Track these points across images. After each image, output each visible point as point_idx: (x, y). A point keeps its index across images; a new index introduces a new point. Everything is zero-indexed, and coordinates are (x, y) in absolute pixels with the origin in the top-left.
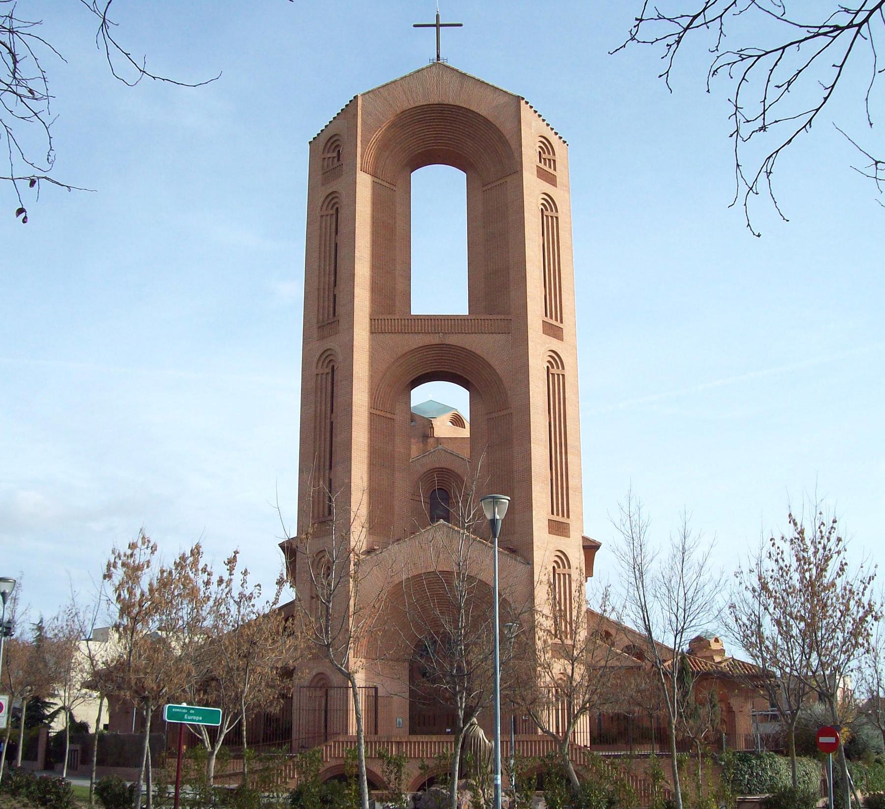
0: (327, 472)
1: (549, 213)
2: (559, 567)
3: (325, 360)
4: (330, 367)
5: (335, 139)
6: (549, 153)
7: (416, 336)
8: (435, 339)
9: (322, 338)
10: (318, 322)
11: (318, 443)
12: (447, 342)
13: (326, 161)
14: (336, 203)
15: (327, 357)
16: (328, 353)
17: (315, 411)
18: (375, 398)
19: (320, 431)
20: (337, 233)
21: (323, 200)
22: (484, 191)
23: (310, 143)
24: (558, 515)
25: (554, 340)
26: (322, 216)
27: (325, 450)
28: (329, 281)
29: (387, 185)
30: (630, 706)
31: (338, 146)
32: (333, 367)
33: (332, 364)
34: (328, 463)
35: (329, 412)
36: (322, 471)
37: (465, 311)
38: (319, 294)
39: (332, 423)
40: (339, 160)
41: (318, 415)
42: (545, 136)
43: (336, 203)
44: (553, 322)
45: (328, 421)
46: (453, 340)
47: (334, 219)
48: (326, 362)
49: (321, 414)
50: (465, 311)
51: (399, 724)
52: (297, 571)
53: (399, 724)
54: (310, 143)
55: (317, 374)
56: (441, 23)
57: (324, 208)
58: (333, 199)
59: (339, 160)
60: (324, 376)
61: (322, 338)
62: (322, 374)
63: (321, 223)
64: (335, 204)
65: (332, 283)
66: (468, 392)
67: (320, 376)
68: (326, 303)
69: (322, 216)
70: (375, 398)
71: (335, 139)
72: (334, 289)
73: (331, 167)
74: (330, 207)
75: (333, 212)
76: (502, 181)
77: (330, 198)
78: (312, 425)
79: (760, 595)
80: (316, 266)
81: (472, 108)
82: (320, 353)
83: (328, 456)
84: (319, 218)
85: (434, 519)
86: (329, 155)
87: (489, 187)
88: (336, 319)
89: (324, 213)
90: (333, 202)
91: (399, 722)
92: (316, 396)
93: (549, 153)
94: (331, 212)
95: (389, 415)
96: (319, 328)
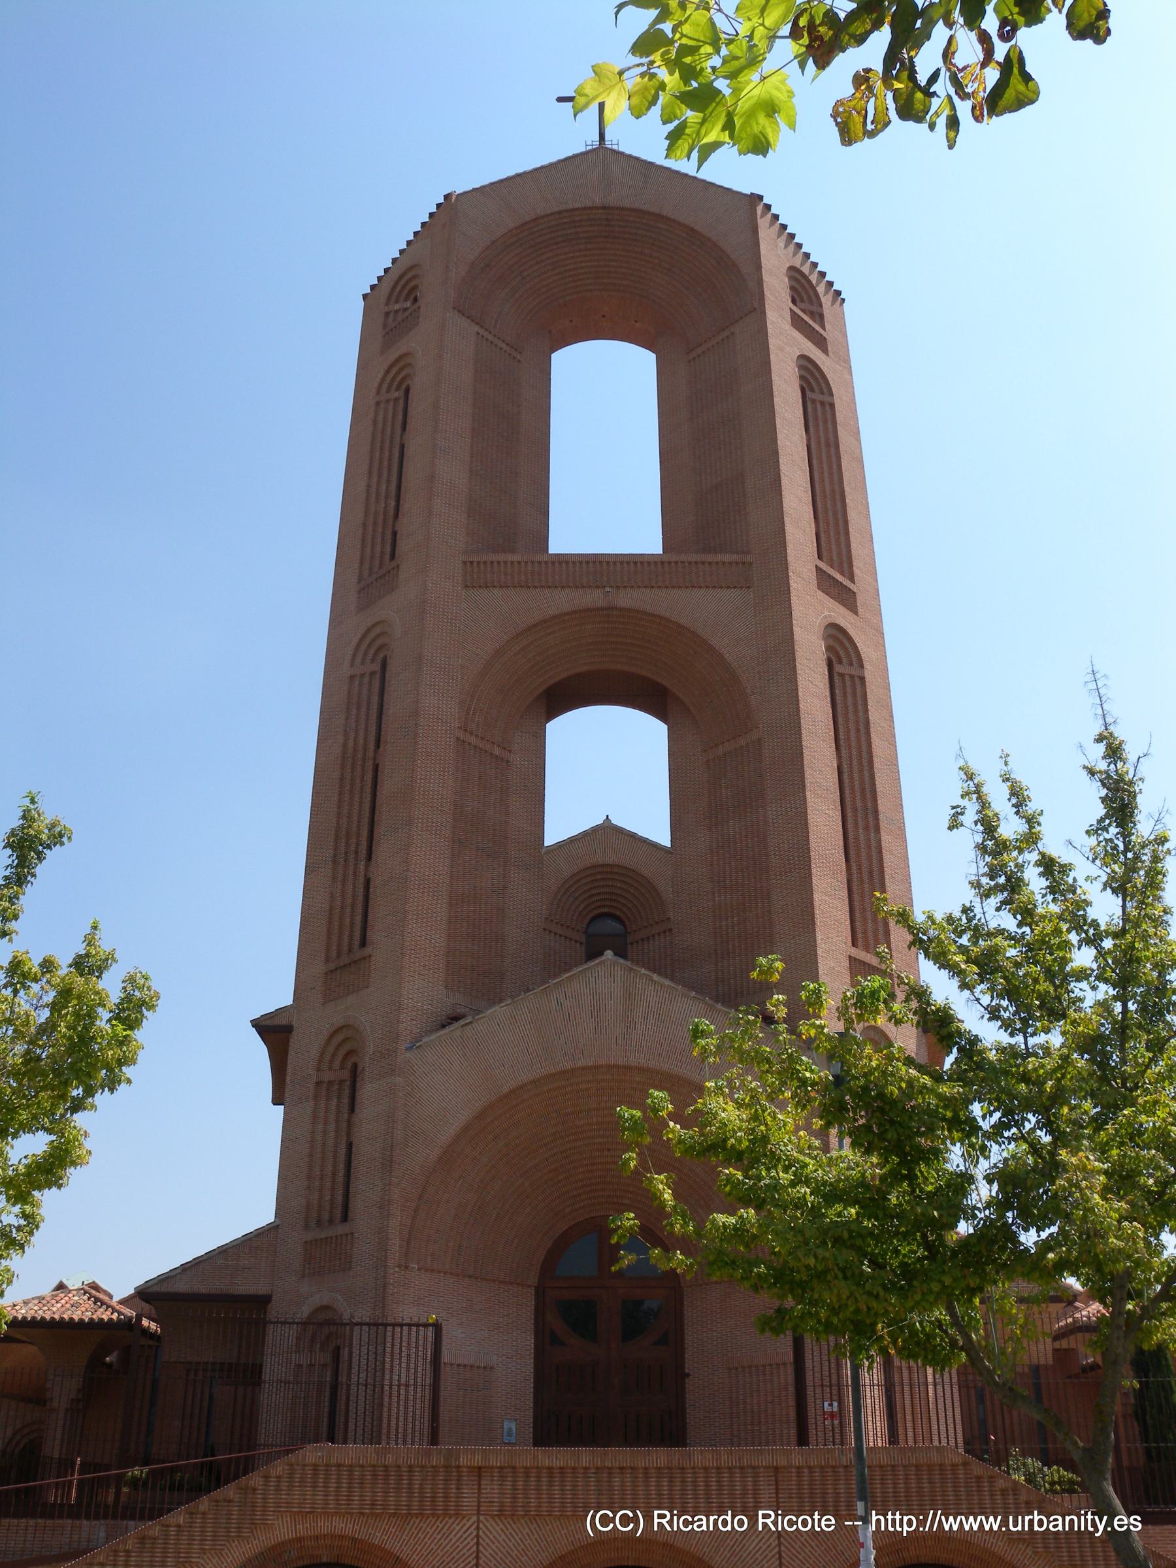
1: (817, 396)
3: (369, 646)
5: (377, 630)
8: (594, 598)
9: (330, 996)
12: (621, 604)
14: (414, 277)
15: (373, 640)
17: (345, 746)
18: (469, 709)
19: (352, 784)
20: (404, 429)
21: (352, 652)
22: (689, 361)
23: (365, 296)
25: (842, 610)
26: (378, 404)
27: (359, 822)
28: (385, 507)
29: (504, 346)
30: (1069, 1180)
32: (355, 1065)
33: (382, 656)
35: (371, 747)
37: (658, 550)
38: (364, 534)
40: (393, 557)
41: (350, 751)
46: (629, 599)
47: (347, 1092)
49: (355, 750)
50: (658, 550)
51: (510, 1435)
52: (288, 1078)
53: (510, 1435)
54: (365, 296)
57: (359, 660)
58: (401, 369)
61: (330, 996)
63: (376, 413)
64: (404, 379)
65: (391, 512)
66: (665, 727)
67: (324, 1086)
68: (378, 548)
69: (352, 677)
70: (469, 709)
72: (394, 522)
73: (345, 959)
75: (401, 393)
76: (727, 333)
81: (664, 213)
83: (365, 833)
85: (593, 953)
86: (397, 307)
87: (699, 351)
88: (368, 950)
89: (327, 1076)
91: (510, 1429)
94: (395, 394)
95: (497, 751)
96: (359, 592)
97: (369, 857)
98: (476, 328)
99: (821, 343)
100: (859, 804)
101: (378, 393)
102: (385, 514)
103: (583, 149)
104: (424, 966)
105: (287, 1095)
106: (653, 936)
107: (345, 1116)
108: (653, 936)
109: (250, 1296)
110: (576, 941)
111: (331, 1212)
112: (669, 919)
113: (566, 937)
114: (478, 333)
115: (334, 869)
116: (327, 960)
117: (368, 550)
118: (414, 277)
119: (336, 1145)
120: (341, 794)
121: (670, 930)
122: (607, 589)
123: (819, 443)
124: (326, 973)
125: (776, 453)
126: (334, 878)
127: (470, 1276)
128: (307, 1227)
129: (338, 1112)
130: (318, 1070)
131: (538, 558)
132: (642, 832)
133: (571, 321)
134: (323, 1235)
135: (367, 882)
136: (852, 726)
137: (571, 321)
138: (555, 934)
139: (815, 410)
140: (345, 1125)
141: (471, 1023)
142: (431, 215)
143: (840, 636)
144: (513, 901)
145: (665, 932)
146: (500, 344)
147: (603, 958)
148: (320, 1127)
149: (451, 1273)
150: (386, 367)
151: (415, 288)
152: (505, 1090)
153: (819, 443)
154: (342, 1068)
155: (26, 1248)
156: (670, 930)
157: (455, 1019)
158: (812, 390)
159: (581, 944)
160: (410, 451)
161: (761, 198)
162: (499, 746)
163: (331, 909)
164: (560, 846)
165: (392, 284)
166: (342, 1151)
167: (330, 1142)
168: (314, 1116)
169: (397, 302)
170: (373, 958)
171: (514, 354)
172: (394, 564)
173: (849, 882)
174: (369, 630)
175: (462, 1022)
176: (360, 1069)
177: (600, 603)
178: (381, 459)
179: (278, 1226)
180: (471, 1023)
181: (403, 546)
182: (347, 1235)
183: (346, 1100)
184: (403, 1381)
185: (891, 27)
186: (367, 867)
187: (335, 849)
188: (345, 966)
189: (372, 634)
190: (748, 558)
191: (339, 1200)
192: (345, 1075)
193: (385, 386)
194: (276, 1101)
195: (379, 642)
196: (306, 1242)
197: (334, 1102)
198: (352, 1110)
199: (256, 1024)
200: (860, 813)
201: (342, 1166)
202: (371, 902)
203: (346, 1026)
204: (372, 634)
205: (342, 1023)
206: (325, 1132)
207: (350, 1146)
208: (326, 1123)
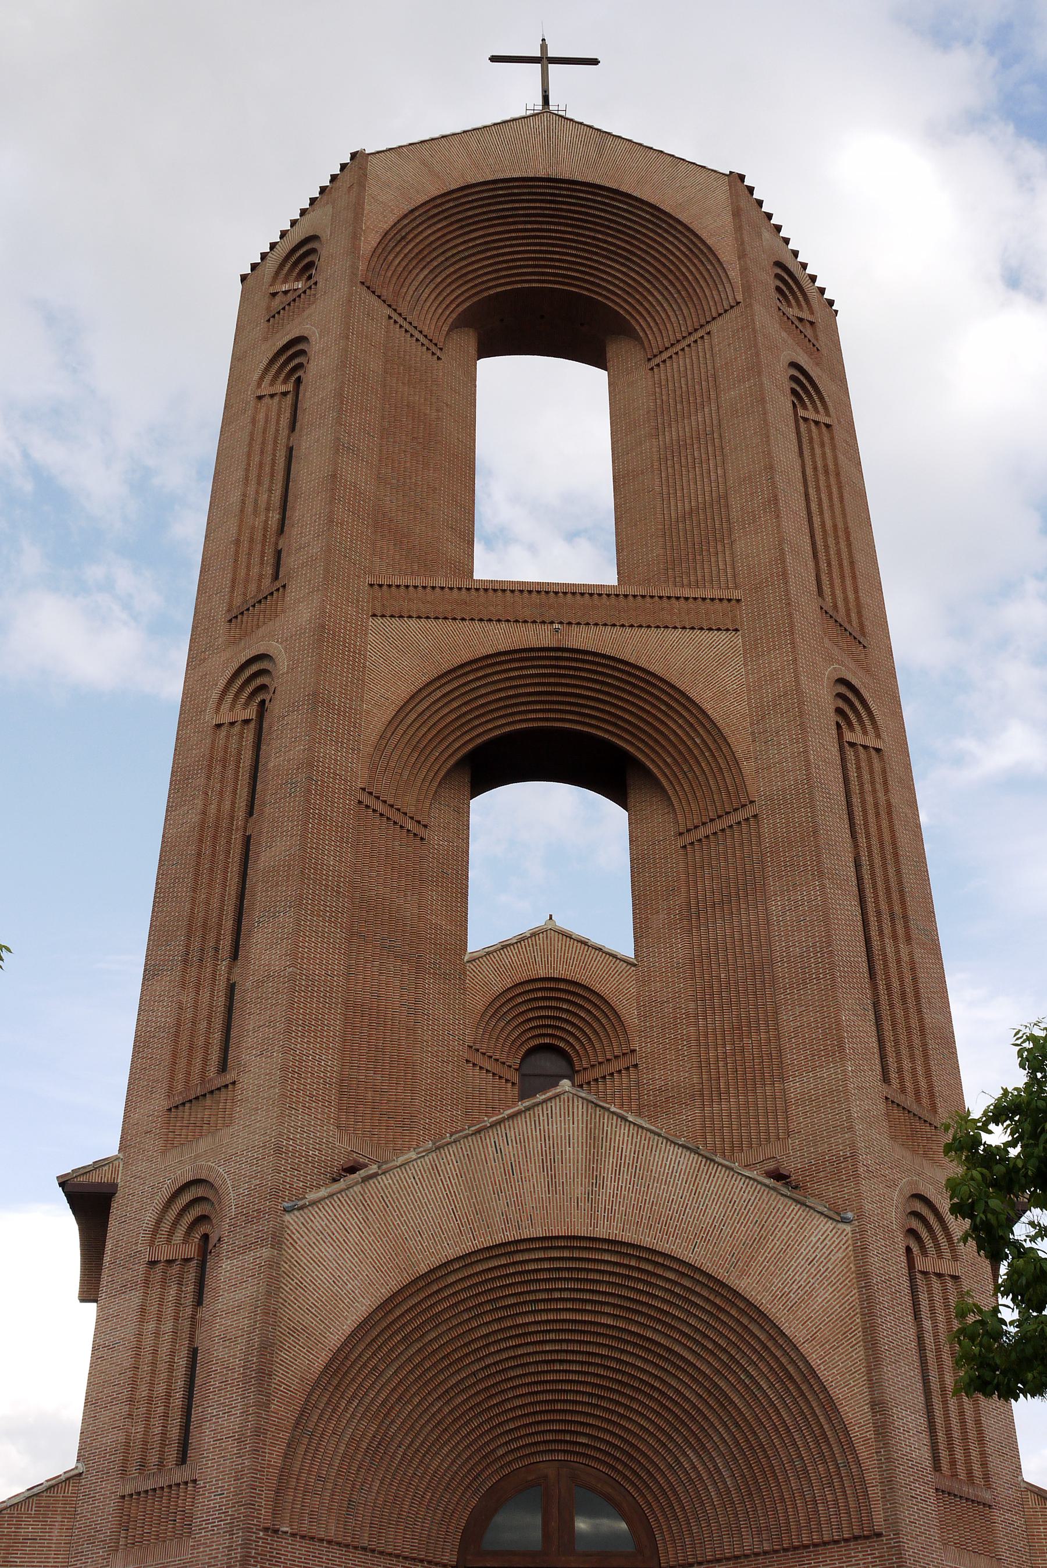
0: (223, 966)
4: (197, 1236)
7: (490, 627)
13: (223, 733)
14: (263, 688)
20: (250, 812)
23: (244, 278)
31: (300, 366)
32: (206, 1237)
34: (226, 943)
35: (241, 814)
36: (209, 963)
37: (614, 582)
39: (247, 841)
43: (263, 688)
45: (237, 837)
46: (582, 638)
47: (191, 1276)
48: (249, 689)
52: (107, 1259)
54: (244, 278)
55: (219, 726)
56: (538, 67)
62: (232, 724)
66: (625, 814)
69: (152, 1263)
77: (254, 668)
78: (192, 850)
80: (235, 497)
82: (228, 674)
83: (229, 924)
84: (142, 1268)
88: (229, 1077)
89: (164, 1253)
90: (259, 681)
92: (209, 778)
97: (235, 956)
98: (388, 311)
99: (813, 349)
100: (884, 907)
101: (259, 385)
102: (265, 529)
103: (523, 114)
104: (311, 1096)
105: (104, 1283)
106: (612, 1074)
107: (189, 1311)
108: (612, 1074)
109: (360, 1326)
110: (507, 1081)
111: (162, 1452)
112: (633, 1051)
113: (494, 1074)
114: (390, 318)
115: (184, 971)
116: (170, 1092)
117: (242, 572)
118: (313, 251)
119: (172, 1353)
120: (197, 874)
121: (636, 1066)
122: (557, 626)
123: (815, 469)
124: (170, 1110)
126: (183, 985)
127: (364, 1549)
128: (124, 1472)
129: (178, 1303)
130: (152, 1244)
131: (466, 584)
132: (596, 938)
133: (502, 320)
134: (149, 1485)
135: (231, 988)
136: (871, 812)
137: (502, 320)
138: (481, 1068)
139: (810, 431)
140: (187, 1323)
141: (375, 1175)
142: (334, 178)
143: (850, 695)
144: (428, 1020)
145: (627, 1069)
146: (417, 334)
147: (558, 1090)
148: (151, 1326)
149: (339, 1544)
150: (270, 355)
151: (311, 265)
152: (423, 1269)
153: (815, 469)
154: (185, 1241)
156: (636, 1066)
157: (352, 1169)
158: (805, 407)
159: (513, 1084)
160: (299, 453)
161: (742, 178)
162: (412, 818)
163: (178, 1024)
164: (488, 953)
166: (181, 1361)
167: (164, 1349)
168: (143, 1310)
169: (285, 282)
170: (239, 1086)
171: (434, 349)
172: (278, 584)
173: (876, 1005)
175: (362, 1173)
176: (213, 1240)
177: (546, 643)
179: (81, 1474)
180: (375, 1175)
181: (290, 562)
182: (186, 1483)
183: (190, 1288)
184: (1026, 1510)
186: (230, 969)
187: (188, 946)
188: (197, 1098)
190: (736, 594)
191: (175, 1433)
192: (191, 1250)
194: (89, 1291)
196: (123, 1497)
197: (173, 1291)
198: (199, 1301)
199: (64, 1183)
200: (886, 917)
201: (180, 1383)
202: (236, 1015)
203: (197, 1182)
205: (189, 1177)
206: (157, 1334)
207: (194, 1353)
208: (159, 1320)
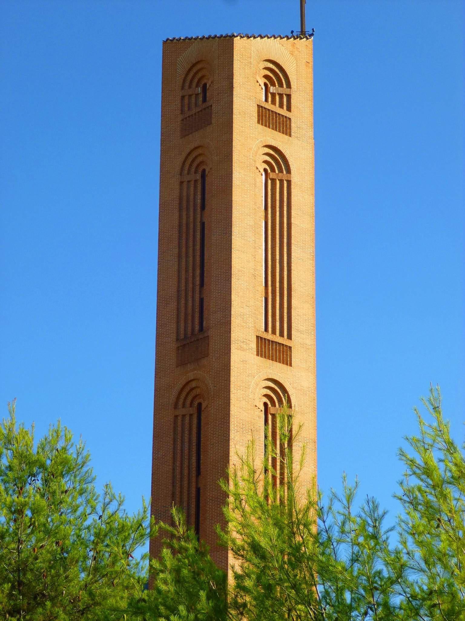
2: (273, 170)
3: (191, 165)
6: (281, 85)
10: (177, 340)
11: (183, 301)
14: (202, 163)
16: (194, 384)
24: (274, 332)
32: (200, 405)
33: (201, 169)
39: (198, 490)
40: (204, 100)
42: (281, 381)
44: (277, 338)
59: (204, 100)
60: (187, 418)
61: (182, 363)
63: (181, 189)
71: (199, 66)
74: (193, 169)
79: (288, 565)
88: (208, 104)
93: (281, 85)
101: (183, 88)
118: (203, 77)
125: (229, 440)
155: (331, 495)
165: (181, 386)
174: (189, 154)
178: (187, 279)
185: (314, 45)
189: (195, 70)
193: (187, 84)
195: (199, 75)
204: (195, 70)
